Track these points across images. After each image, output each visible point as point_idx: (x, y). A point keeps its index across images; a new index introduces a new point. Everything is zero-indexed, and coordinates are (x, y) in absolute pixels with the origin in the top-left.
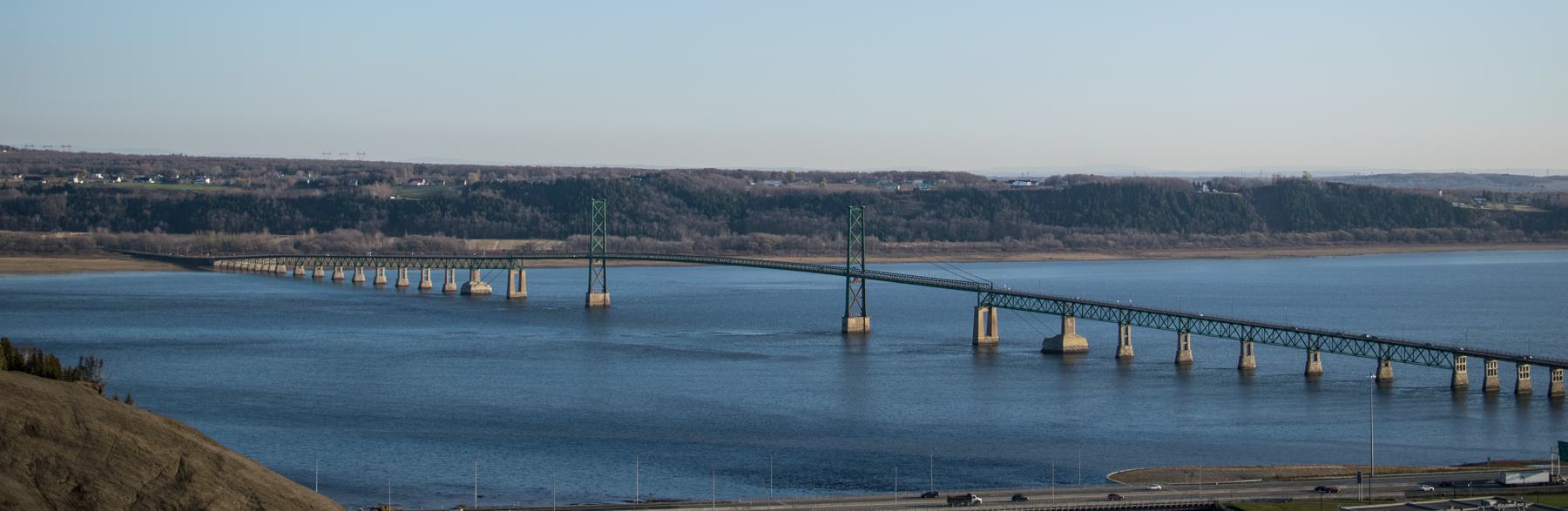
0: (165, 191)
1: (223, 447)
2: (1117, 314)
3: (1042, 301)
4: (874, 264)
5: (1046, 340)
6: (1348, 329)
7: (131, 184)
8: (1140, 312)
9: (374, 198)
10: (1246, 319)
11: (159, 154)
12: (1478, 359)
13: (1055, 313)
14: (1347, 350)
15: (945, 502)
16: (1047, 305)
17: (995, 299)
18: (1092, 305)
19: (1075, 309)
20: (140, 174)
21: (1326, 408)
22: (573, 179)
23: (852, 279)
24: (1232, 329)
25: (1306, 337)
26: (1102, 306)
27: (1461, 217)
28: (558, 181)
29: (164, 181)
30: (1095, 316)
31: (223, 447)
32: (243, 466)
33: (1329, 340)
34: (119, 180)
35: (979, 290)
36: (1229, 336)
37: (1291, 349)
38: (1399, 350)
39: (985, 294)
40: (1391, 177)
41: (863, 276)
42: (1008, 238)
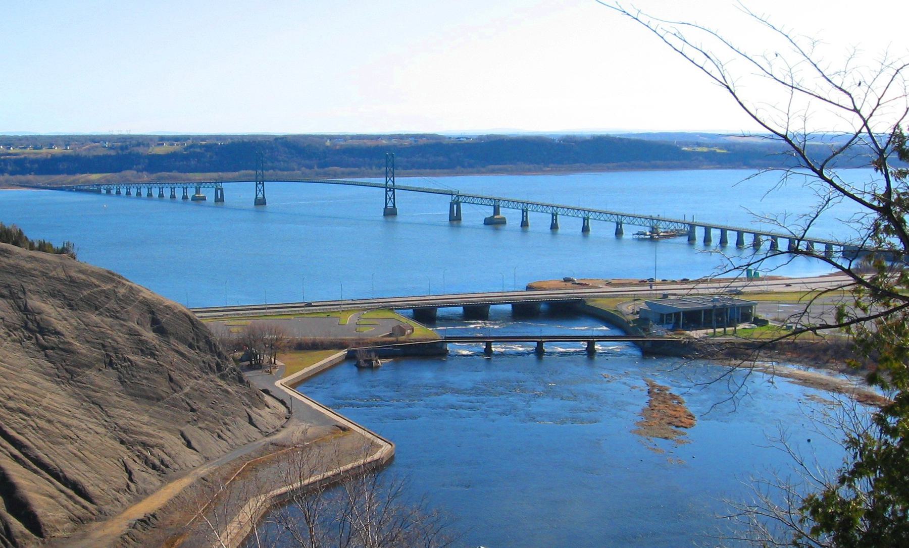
0: (36, 154)
1: (132, 283)
2: (521, 205)
3: (484, 199)
4: (400, 181)
5: (486, 219)
6: (637, 213)
7: (17, 151)
8: (504, 201)
9: (140, 154)
10: (616, 212)
11: (29, 135)
12: (822, 244)
13: (490, 205)
14: (539, 210)
15: (440, 312)
16: (485, 202)
17: (460, 199)
18: (538, 205)
19: (529, 206)
20: (21, 145)
21: (130, 454)
22: (240, 142)
23: (388, 189)
24: (569, 212)
25: (616, 217)
26: (533, 204)
27: (687, 155)
28: (232, 142)
29: (34, 148)
30: (539, 210)
31: (132, 283)
32: (142, 291)
33: (627, 218)
34: (11, 148)
35: (452, 195)
36: (547, 212)
37: (608, 222)
38: (627, 219)
39: (455, 196)
40: (648, 134)
41: (393, 189)
42: (458, 167)
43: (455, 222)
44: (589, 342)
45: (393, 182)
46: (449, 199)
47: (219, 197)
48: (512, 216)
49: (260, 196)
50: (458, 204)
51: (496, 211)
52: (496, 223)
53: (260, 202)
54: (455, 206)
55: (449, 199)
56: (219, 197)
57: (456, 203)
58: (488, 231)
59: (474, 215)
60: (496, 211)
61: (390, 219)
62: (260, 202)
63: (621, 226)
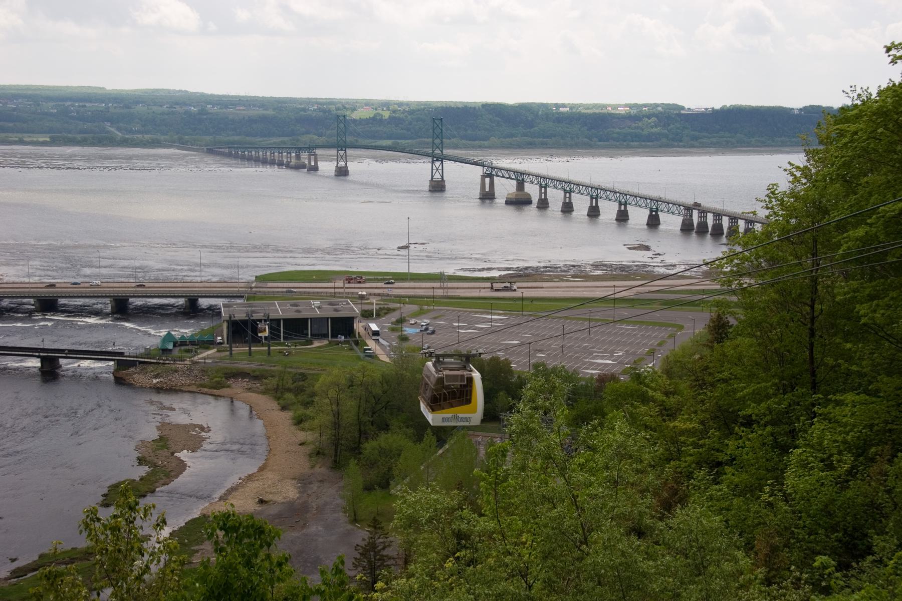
35: (483, 166)
43: (488, 201)
44: (43, 360)
45: (442, 152)
46: (479, 171)
47: (487, 189)
48: (532, 190)
49: (437, 176)
50: (491, 176)
51: (520, 185)
52: (519, 202)
53: (438, 187)
54: (487, 180)
55: (479, 171)
56: (487, 189)
57: (490, 175)
58: (511, 211)
59: (505, 187)
60: (520, 185)
61: (437, 194)
62: (438, 187)
63: (625, 207)
